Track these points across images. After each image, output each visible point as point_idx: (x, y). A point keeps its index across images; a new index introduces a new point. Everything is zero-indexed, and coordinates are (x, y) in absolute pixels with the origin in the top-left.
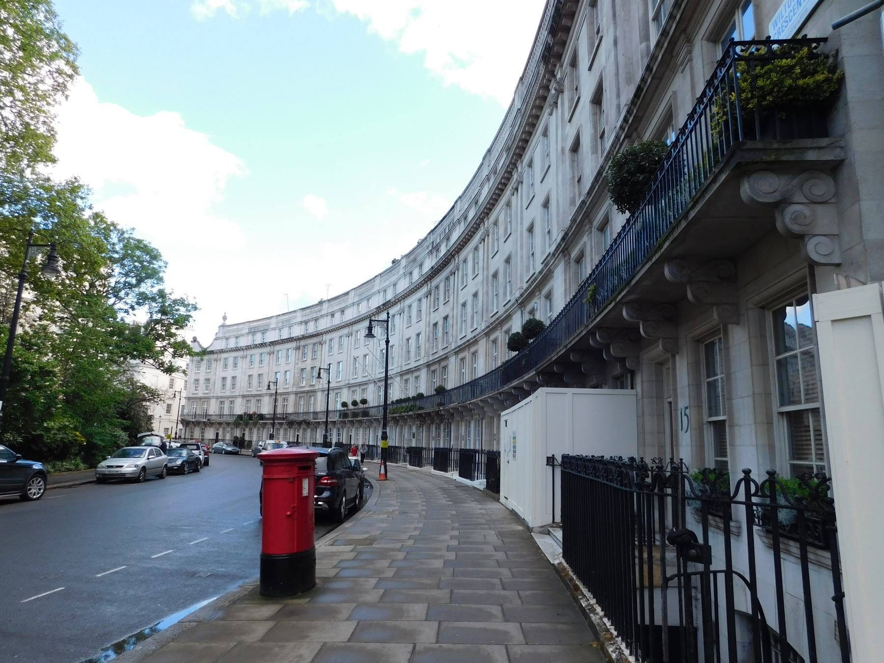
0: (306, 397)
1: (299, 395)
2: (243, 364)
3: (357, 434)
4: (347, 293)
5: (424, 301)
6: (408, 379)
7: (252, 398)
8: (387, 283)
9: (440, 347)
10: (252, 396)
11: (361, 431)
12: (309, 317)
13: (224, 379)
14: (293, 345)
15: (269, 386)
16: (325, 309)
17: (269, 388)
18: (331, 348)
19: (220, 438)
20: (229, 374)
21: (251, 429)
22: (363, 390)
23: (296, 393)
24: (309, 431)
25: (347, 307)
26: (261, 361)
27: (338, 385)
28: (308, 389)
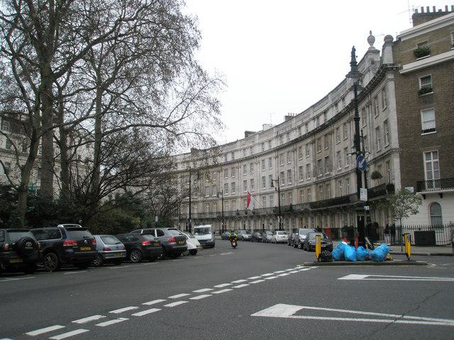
2: (257, 168)
3: (326, 221)
8: (265, 139)
12: (319, 112)
13: (245, 181)
14: (274, 155)
16: (294, 123)
17: (272, 186)
20: (248, 178)
22: (328, 185)
23: (316, 183)
24: (329, 218)
25: (328, 109)
26: (270, 164)
28: (288, 187)
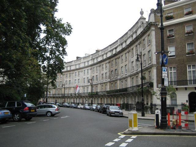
0: (113, 84)
1: (111, 83)
3: (114, 100)
4: (72, 62)
5: (138, 46)
6: (133, 78)
7: (103, 84)
9: (147, 64)
10: (85, 86)
11: (69, 99)
15: (89, 81)
18: (76, 75)
19: (93, 102)
20: (77, 78)
21: (67, 99)
27: (106, 81)
28: (96, 83)
